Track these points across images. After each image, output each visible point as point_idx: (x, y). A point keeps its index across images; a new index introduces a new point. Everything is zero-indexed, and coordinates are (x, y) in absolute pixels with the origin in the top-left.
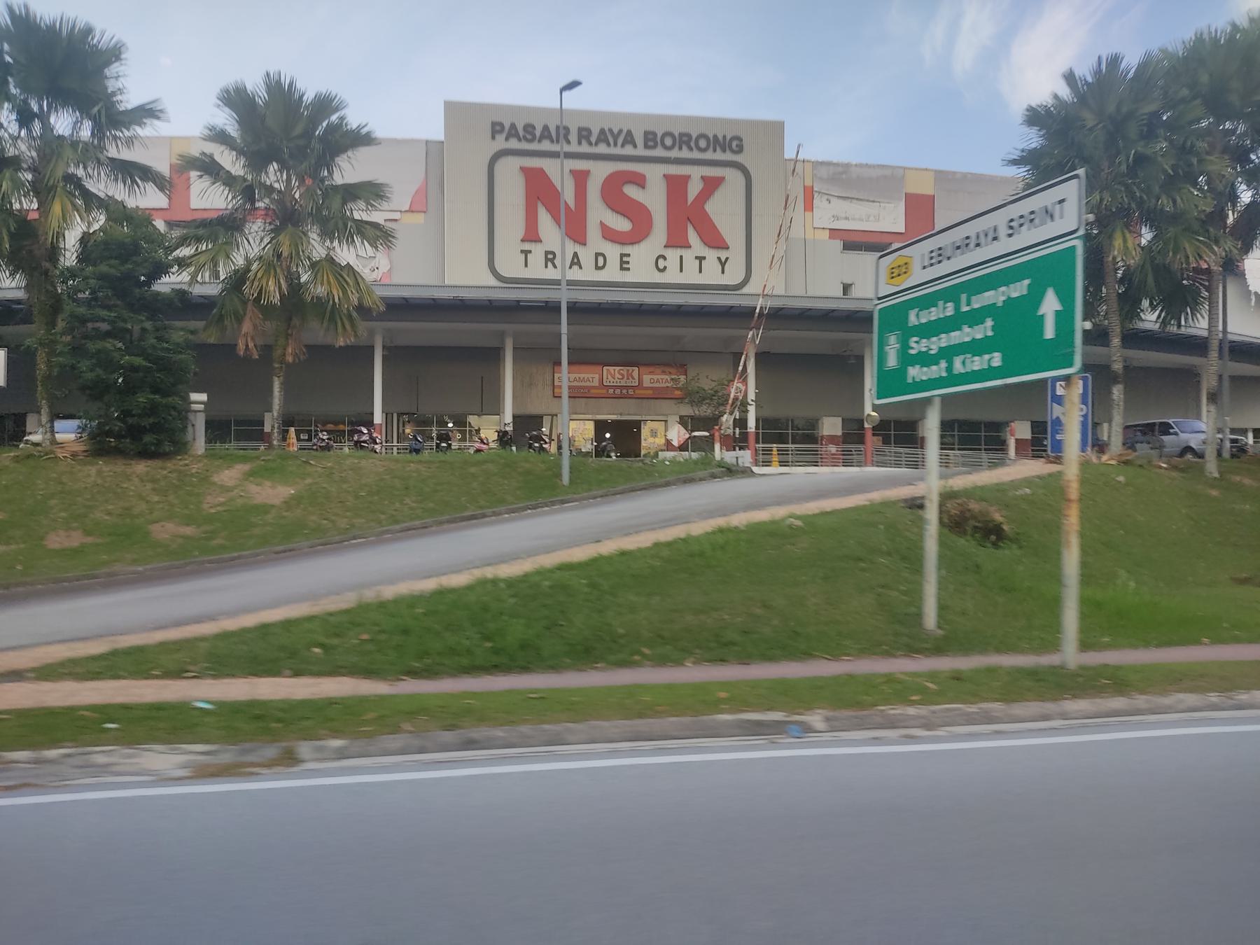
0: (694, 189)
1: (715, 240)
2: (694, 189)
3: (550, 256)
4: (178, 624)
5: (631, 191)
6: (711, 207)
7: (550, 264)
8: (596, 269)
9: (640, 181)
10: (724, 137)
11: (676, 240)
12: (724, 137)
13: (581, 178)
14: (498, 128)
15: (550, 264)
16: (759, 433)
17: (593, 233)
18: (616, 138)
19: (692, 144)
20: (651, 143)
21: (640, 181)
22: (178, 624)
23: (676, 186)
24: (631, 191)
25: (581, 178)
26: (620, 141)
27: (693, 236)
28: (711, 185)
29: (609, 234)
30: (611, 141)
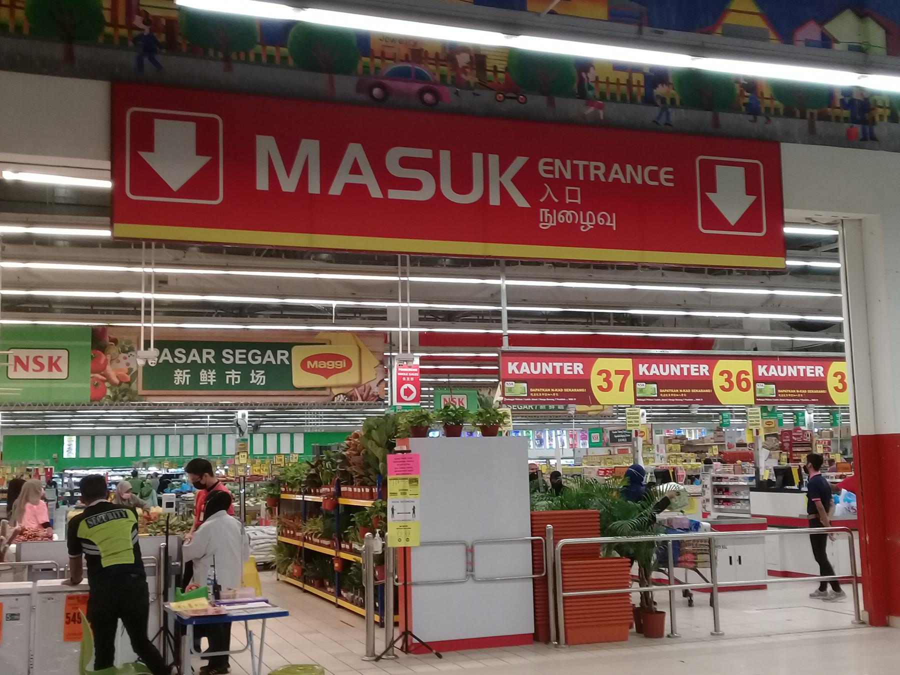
6: (59, 363)
27: (54, 368)
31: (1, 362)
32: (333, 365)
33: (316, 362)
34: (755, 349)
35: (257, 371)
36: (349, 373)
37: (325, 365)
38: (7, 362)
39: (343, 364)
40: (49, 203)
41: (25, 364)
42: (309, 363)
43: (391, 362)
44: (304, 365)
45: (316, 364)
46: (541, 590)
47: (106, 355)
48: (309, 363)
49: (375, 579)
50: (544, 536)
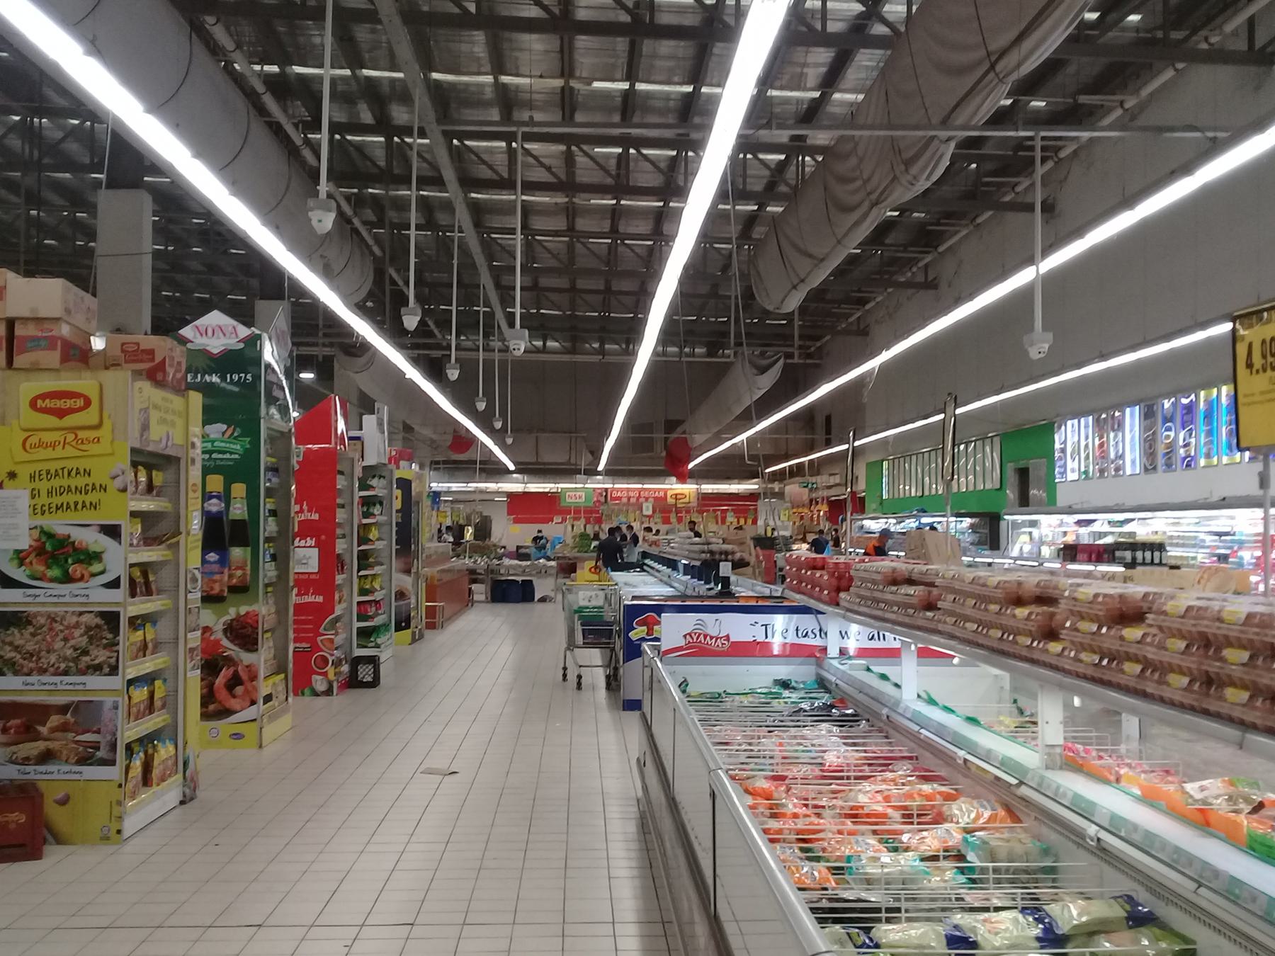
31: (1270, 615)
32: (69, 403)
33: (47, 401)
34: (990, 564)
35: (300, 125)
36: (689, 821)
37: (59, 404)
38: (361, 429)
39: (80, 403)
40: (33, 497)
41: (495, 177)
42: (39, 402)
43: (1232, 664)
44: (88, 403)
45: (48, 403)
46: (988, 449)
47: (1039, 528)
48: (39, 402)
49: (207, 496)
50: (609, 472)
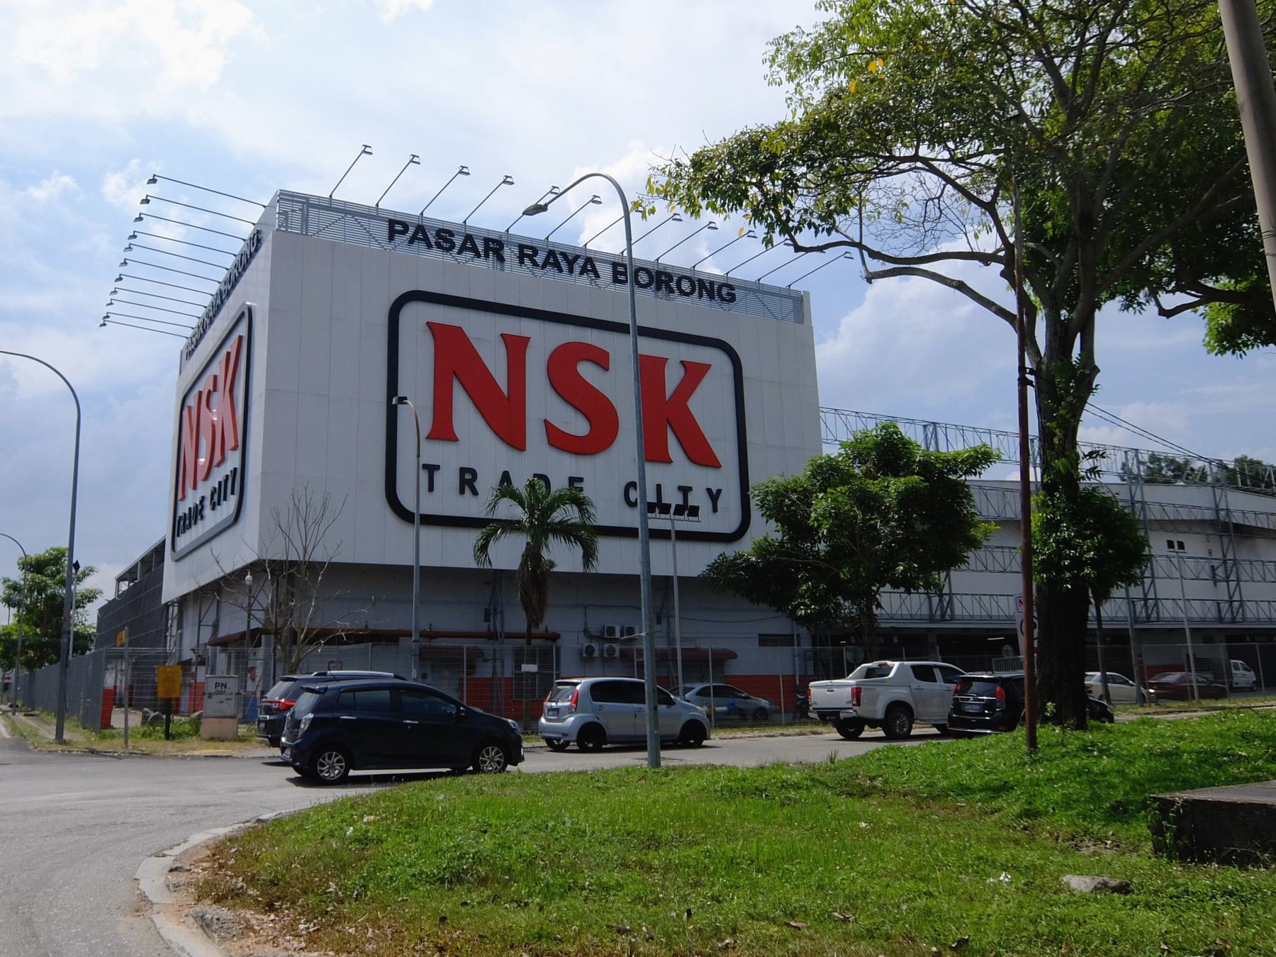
0: (673, 377)
1: (702, 455)
2: (673, 377)
3: (468, 476)
4: (399, 779)
5: (587, 371)
6: (695, 404)
7: (467, 490)
8: (570, 478)
9: (601, 359)
10: (701, 296)
11: (653, 452)
12: (701, 296)
13: (516, 347)
14: (398, 227)
15: (467, 490)
16: (1228, 678)
17: (535, 434)
18: (571, 264)
19: (673, 285)
20: (622, 278)
21: (601, 359)
22: (399, 779)
23: (649, 370)
24: (587, 371)
25: (516, 347)
26: (577, 269)
28: (694, 373)
29: (558, 439)
30: (564, 265)
